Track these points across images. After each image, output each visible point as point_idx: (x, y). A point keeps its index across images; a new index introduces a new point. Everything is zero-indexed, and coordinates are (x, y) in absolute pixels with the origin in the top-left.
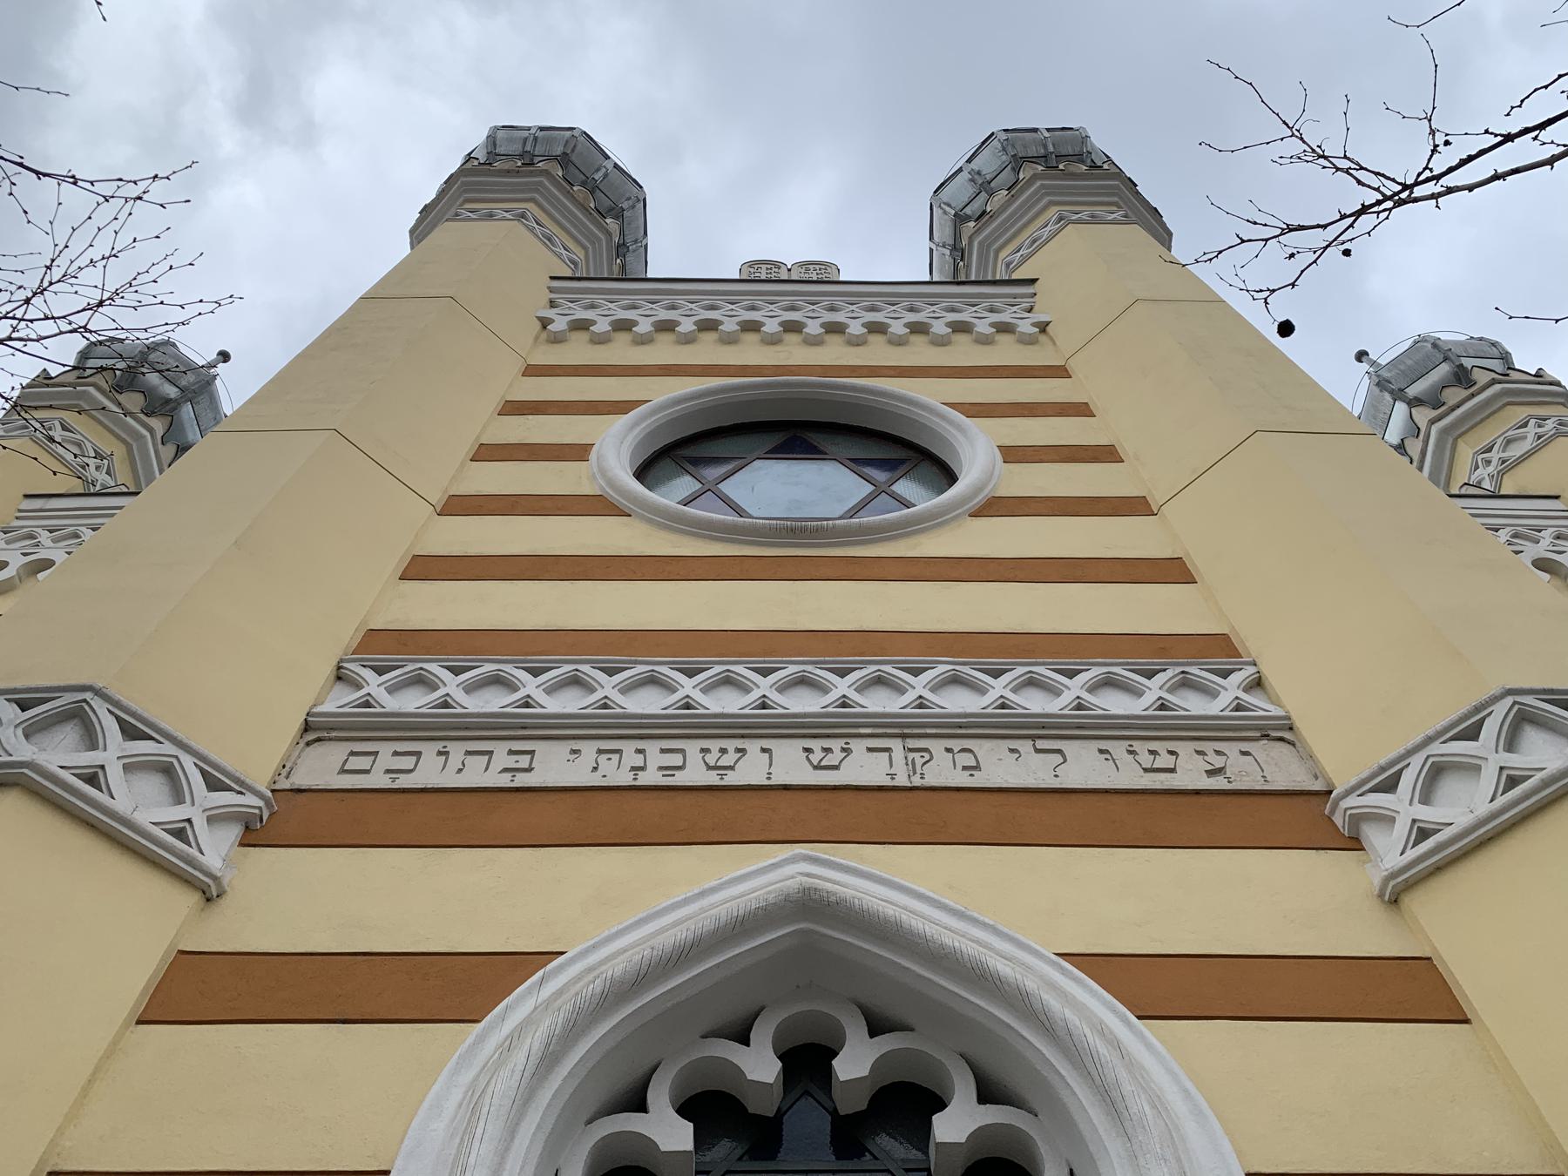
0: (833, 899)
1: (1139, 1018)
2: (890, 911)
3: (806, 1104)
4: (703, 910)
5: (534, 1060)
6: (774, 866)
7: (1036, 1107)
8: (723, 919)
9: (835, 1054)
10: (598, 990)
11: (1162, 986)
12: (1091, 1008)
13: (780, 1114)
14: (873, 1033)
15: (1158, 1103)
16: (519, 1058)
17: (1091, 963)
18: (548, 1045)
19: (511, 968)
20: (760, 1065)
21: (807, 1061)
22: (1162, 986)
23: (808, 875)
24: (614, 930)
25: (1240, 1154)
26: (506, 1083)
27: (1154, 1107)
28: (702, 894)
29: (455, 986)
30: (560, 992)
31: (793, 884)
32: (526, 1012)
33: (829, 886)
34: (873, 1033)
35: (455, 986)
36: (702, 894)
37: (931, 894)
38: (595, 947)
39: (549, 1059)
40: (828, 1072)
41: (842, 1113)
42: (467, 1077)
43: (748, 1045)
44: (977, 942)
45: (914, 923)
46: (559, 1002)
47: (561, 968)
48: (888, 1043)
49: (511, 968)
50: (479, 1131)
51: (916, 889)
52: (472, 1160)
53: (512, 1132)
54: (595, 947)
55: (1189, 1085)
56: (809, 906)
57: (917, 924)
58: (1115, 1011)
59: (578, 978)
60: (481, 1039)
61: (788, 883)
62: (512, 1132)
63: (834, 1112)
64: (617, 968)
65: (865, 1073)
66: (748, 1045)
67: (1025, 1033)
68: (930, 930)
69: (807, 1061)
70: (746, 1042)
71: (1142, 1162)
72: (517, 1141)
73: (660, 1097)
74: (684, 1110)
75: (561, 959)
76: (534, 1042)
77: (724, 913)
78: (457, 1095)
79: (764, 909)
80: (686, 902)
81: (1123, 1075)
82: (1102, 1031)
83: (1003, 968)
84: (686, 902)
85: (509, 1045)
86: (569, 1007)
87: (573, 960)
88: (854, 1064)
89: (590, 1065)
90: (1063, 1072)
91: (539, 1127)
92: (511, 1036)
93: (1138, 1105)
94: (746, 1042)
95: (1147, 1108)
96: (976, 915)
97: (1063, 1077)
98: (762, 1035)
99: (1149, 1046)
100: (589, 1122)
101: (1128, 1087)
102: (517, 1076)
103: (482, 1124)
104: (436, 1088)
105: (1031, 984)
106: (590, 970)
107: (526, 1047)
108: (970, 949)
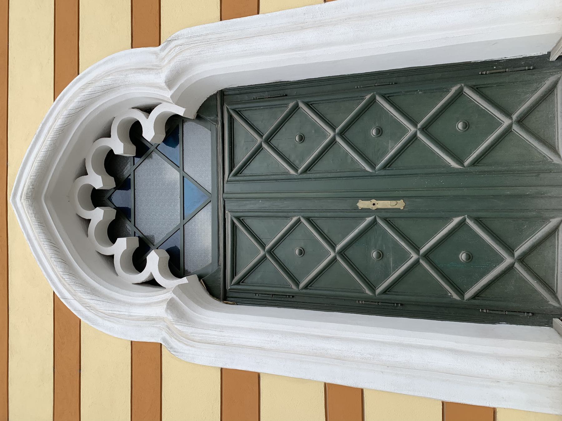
0: (31, 187)
1: (78, 74)
2: (36, 164)
3: (114, 199)
4: (36, 239)
5: (94, 297)
6: (20, 216)
7: (111, 118)
8: (39, 231)
9: (94, 188)
10: (68, 277)
11: (66, 64)
12: (74, 91)
13: (116, 208)
14: (109, 136)
15: (108, 73)
16: (92, 303)
17: (57, 89)
18: (88, 293)
19: (58, 307)
20: (98, 215)
21: (98, 198)
22: (66, 64)
23: (21, 197)
24: (44, 273)
25: (125, 49)
26: (101, 306)
27: (109, 75)
28: (30, 239)
29: (67, 330)
30: (69, 291)
31: (25, 203)
32: (75, 303)
33: (25, 189)
34: (109, 136)
35: (67, 330)
36: (30, 239)
37: (29, 148)
38: (51, 280)
39: (93, 292)
40: (99, 190)
41: (115, 186)
42: (100, 320)
43: (90, 220)
44: (49, 131)
45: (41, 155)
46: (73, 291)
47: (60, 292)
48: (90, 169)
49: (58, 307)
50: (118, 313)
51: (26, 158)
52: (127, 313)
53: (118, 301)
54: (51, 280)
55: (102, 61)
56: (34, 196)
57: (42, 154)
58: (76, 83)
59: (64, 285)
60: (86, 318)
61: (24, 205)
62: (118, 301)
63: (116, 189)
64: (59, 270)
65: (100, 177)
66: (90, 220)
67: (84, 118)
68: (44, 149)
69: (98, 198)
70: (89, 220)
71: (127, 83)
72: (122, 299)
73: (108, 250)
74: (114, 241)
75: (56, 293)
76: (86, 298)
77: (37, 231)
78: (107, 323)
79: (35, 214)
80: (33, 246)
81: (98, 84)
82: (83, 89)
83: (59, 122)
84: (33, 246)
85: (88, 307)
86: (74, 287)
87: (57, 288)
88: (97, 180)
89: (118, 289)
90: (98, 106)
91: (117, 292)
92: (85, 307)
93: (108, 80)
94: (89, 220)
95: (110, 78)
96: (38, 131)
97: (100, 106)
98: (87, 214)
99: (89, 73)
100: (117, 275)
101: (102, 83)
102: (98, 302)
103: (115, 312)
104: (104, 331)
105: (65, 113)
106: (60, 281)
107: (89, 301)
108: (51, 135)
